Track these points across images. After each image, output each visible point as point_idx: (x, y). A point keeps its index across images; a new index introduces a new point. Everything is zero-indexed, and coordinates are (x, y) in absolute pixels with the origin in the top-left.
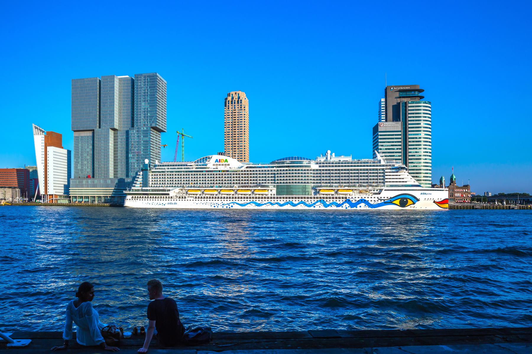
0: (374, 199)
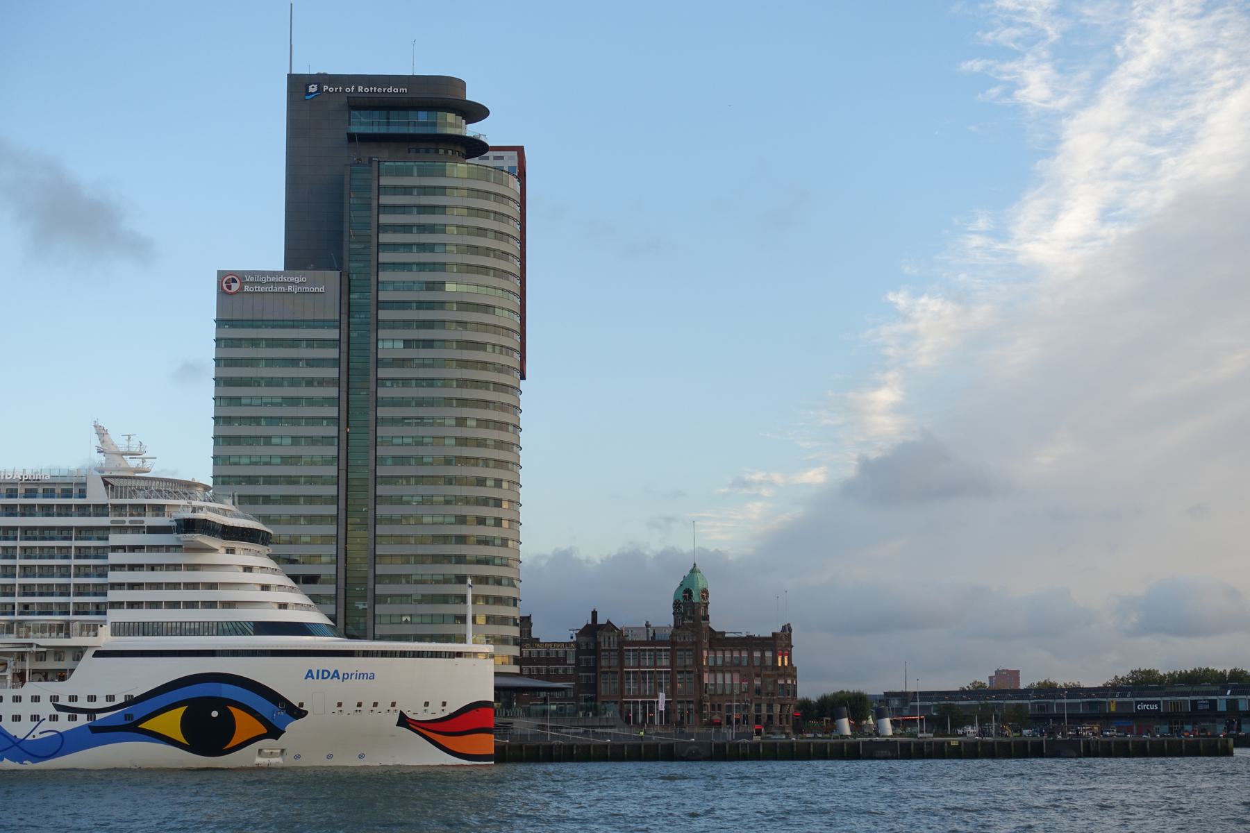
0: (36, 709)
